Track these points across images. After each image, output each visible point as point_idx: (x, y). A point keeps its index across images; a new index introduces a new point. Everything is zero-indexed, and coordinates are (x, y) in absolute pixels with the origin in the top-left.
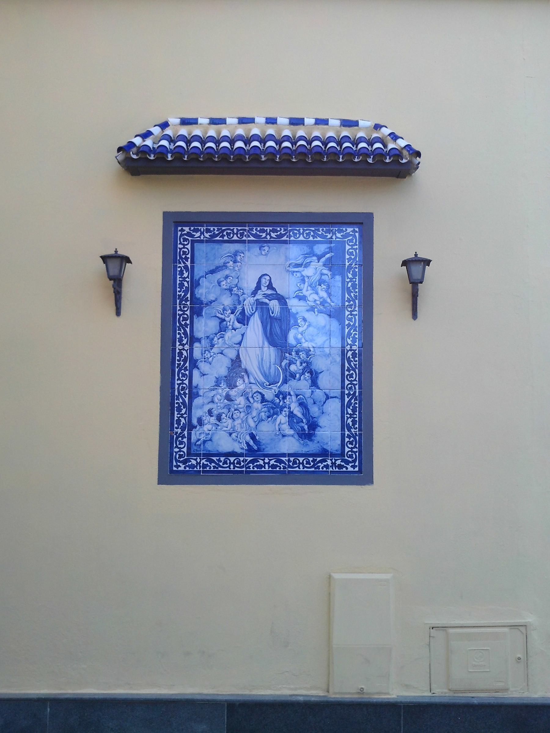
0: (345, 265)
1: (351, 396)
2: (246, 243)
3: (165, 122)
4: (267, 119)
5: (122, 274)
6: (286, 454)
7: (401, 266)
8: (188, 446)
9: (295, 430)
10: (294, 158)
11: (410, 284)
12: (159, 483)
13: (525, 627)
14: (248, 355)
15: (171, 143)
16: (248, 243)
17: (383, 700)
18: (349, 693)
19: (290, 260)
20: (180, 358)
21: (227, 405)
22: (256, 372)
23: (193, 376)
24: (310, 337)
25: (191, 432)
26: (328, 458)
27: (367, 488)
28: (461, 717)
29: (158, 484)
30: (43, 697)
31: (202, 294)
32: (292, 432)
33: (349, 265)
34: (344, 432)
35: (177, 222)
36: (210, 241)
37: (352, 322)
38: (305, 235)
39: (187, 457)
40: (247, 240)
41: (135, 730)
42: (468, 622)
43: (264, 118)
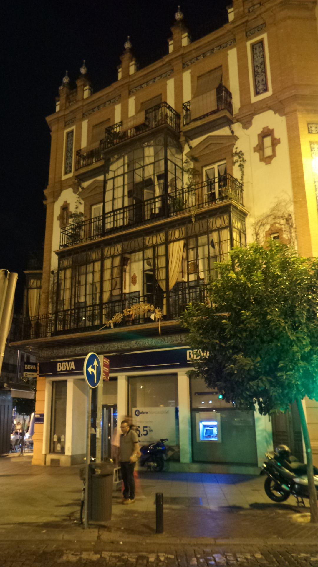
2: (161, 327)
7: (163, 94)
9: (184, 300)
10: (67, 73)
11: (241, 151)
13: (195, 459)
15: (234, 161)
16: (158, 328)
18: (87, 442)
19: (92, 389)
20: (71, 217)
22: (202, 225)
25: (213, 430)
28: (290, 483)
30: (280, 539)
31: (304, 479)
34: (10, 345)
37: (65, 208)
39: (214, 168)
41: (52, 317)
42: (185, 215)
43: (173, 473)
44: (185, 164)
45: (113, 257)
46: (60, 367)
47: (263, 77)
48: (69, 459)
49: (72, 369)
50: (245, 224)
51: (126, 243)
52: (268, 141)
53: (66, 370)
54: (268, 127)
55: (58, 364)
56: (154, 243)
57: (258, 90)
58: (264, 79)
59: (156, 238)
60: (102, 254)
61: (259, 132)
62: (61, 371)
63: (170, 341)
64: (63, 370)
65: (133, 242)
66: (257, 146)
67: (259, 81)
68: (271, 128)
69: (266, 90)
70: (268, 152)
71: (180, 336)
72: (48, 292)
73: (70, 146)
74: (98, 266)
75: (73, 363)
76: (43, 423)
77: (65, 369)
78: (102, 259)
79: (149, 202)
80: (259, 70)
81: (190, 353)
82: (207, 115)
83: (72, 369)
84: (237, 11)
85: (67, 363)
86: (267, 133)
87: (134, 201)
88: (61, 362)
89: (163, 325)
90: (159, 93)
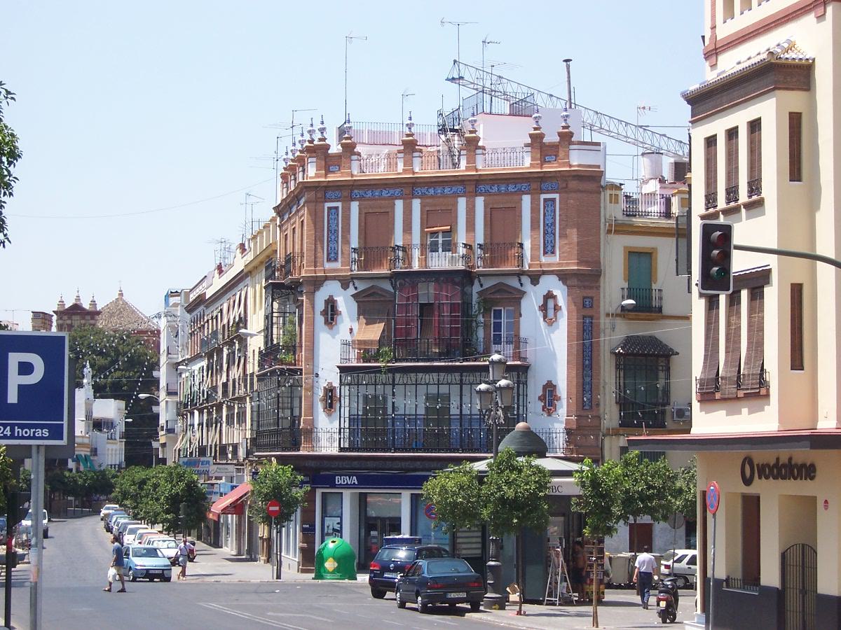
0: (711, 66)
1: (265, 233)
3: (750, 209)
4: (170, 581)
5: (231, 389)
6: (475, 163)
8: (798, 368)
12: (790, 113)
14: (646, 126)
17: (575, 383)
21: (754, 278)
23: (777, 11)
24: (112, 333)
25: (758, 465)
26: (636, 545)
27: (792, 282)
29: (19, 385)
32: (110, 460)
33: (426, 478)
35: (677, 272)
36: (572, 430)
38: (21, 550)
40: (62, 422)
44: (298, 493)
46: (339, 480)
47: (552, 238)
49: (354, 483)
50: (525, 383)
52: (551, 303)
53: (347, 484)
55: (337, 477)
57: (369, 544)
60: (461, 380)
64: (343, 483)
66: (324, 310)
70: (551, 313)
73: (333, 226)
75: (355, 478)
77: (345, 483)
78: (461, 384)
80: (550, 230)
82: (740, 38)
83: (354, 483)
85: (348, 477)
86: (549, 296)
89: (553, 258)
90: (714, 133)
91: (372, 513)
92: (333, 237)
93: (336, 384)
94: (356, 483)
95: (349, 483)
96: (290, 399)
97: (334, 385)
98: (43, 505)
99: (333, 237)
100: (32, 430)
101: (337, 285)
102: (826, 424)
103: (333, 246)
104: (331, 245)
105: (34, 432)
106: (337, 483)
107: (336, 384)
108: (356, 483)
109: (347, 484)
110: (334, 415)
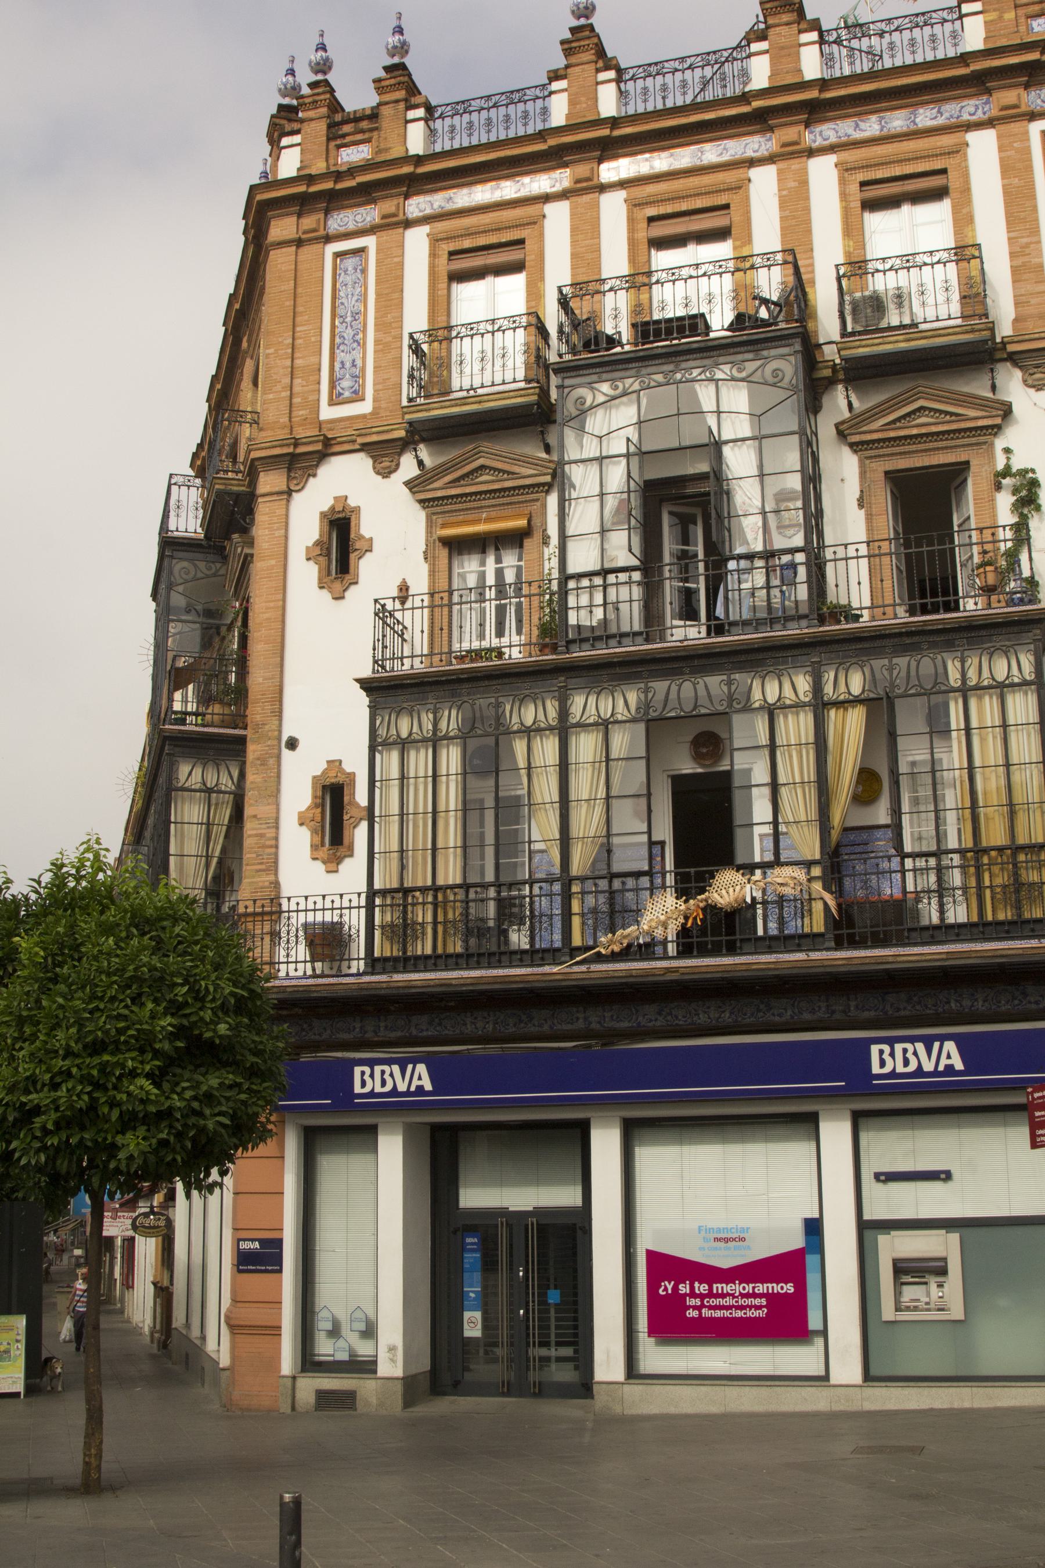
40: (738, 932)
45: (605, 726)
48: (399, 1387)
51: (660, 686)
53: (394, 1092)
54: (321, 513)
55: (357, 1070)
56: (404, 734)
58: (359, 363)
59: (776, 683)
60: (564, 713)
61: (325, 508)
62: (372, 1094)
63: (789, 1013)
65: (687, 686)
66: (317, 543)
67: (342, 363)
68: (352, 502)
69: (358, 397)
71: (581, 1009)
72: (530, 805)
73: (349, 303)
74: (547, 750)
75: (421, 1068)
76: (280, 1271)
77: (913, 1066)
78: (564, 730)
79: (585, 582)
81: (363, 1073)
84: (993, 16)
85: (396, 1069)
87: (245, 994)
88: (371, 1063)
91: (867, 1216)
92: (349, 333)
93: (357, 764)
94: (428, 1087)
95: (402, 1087)
96: (611, 578)
97: (348, 768)
98: (891, 468)
99: (349, 333)
100: (751, 1285)
101: (361, 463)
102: (1040, 840)
103: (348, 359)
104: (340, 356)
105: (754, 1288)
106: (876, 1069)
107: (357, 764)
108: (428, 1087)
109: (394, 1092)
110: (347, 865)
